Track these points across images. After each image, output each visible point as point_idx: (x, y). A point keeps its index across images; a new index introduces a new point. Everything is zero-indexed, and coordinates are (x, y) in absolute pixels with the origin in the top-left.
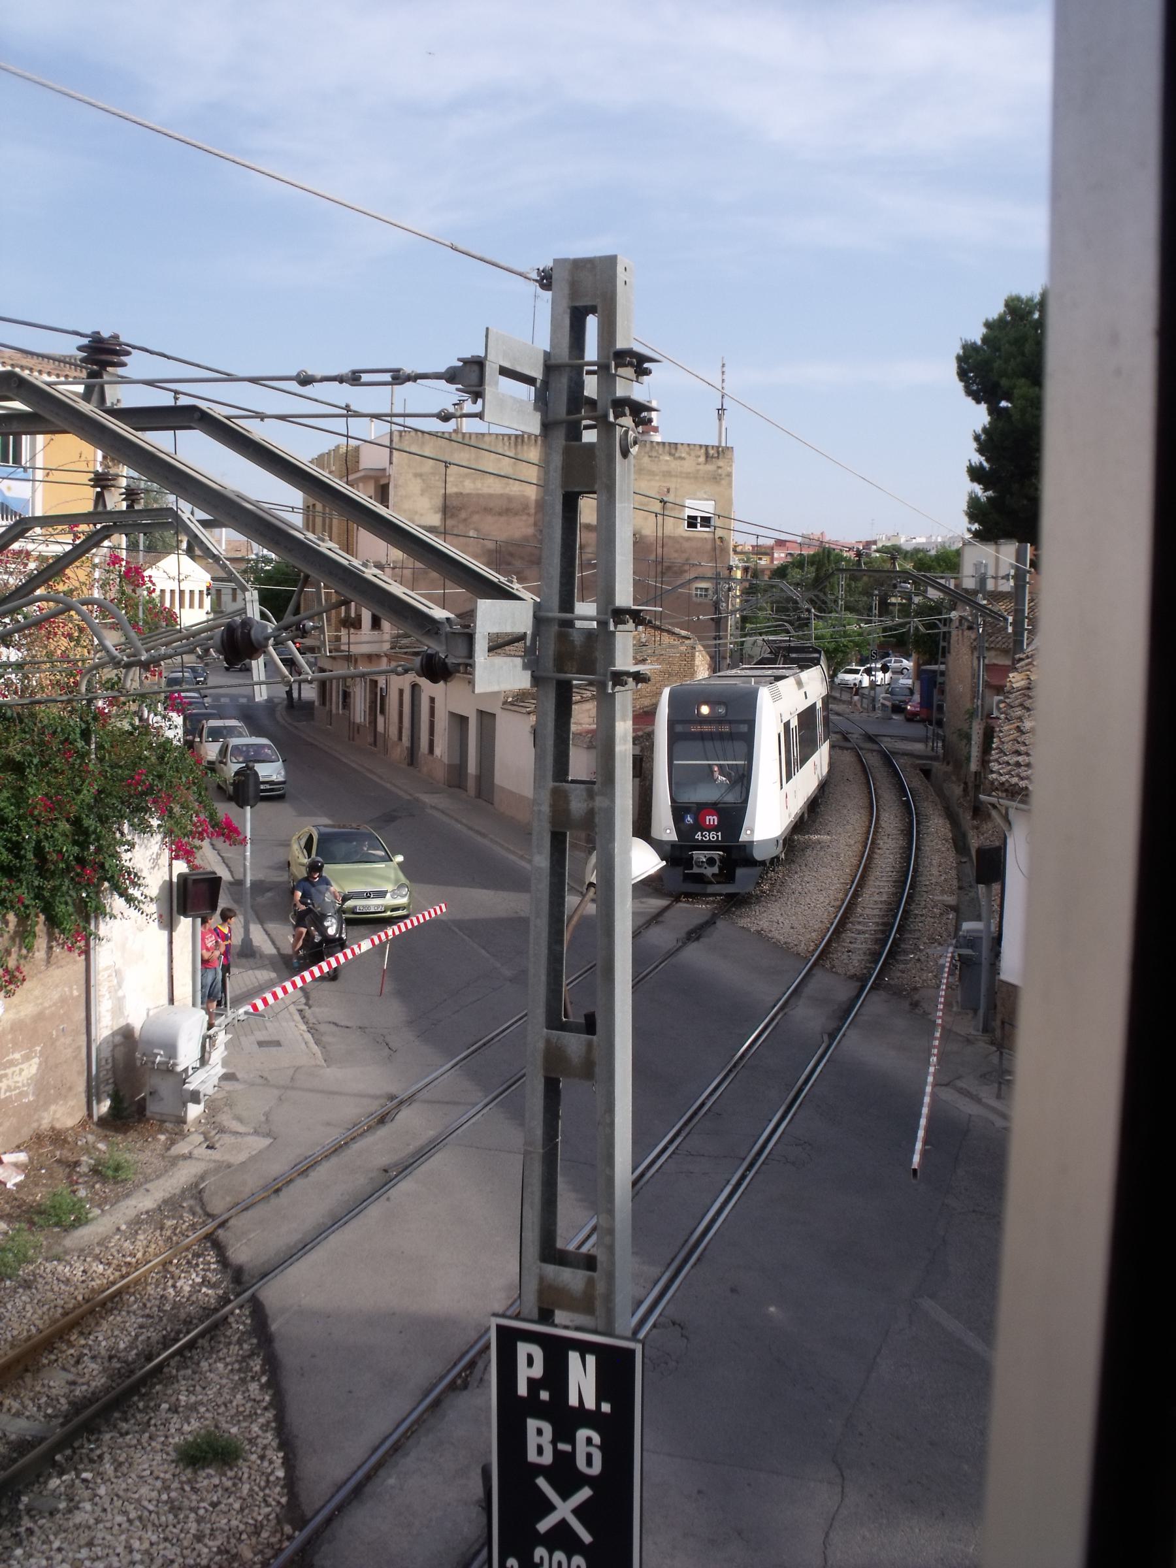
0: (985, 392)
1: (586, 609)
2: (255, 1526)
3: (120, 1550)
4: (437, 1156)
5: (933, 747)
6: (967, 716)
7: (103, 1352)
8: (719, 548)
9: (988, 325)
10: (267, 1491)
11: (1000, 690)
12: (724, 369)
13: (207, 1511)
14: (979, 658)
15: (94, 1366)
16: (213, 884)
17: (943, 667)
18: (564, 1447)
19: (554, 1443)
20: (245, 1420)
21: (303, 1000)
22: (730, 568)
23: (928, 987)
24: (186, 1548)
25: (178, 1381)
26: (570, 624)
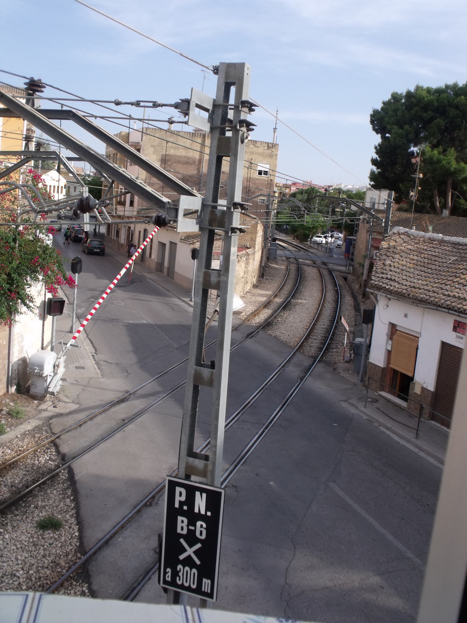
0: (380, 130)
1: (222, 202)
2: (66, 553)
3: (13, 559)
4: (144, 415)
5: (349, 269)
6: (363, 258)
7: (9, 484)
8: (270, 184)
9: (384, 103)
10: (71, 540)
11: (377, 248)
12: (278, 113)
13: (47, 546)
14: (370, 235)
15: (5, 489)
16: (61, 303)
17: (355, 238)
18: (192, 528)
19: (188, 526)
20: (64, 513)
21: (94, 352)
22: (274, 192)
23: (340, 362)
24: (39, 560)
25: (38, 497)
26: (215, 207)
